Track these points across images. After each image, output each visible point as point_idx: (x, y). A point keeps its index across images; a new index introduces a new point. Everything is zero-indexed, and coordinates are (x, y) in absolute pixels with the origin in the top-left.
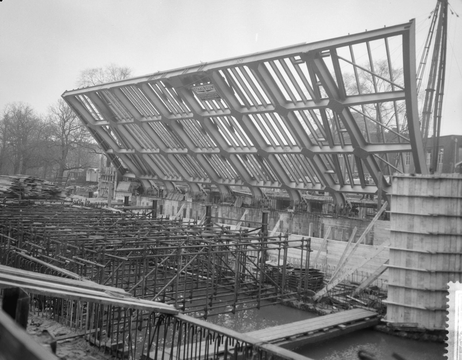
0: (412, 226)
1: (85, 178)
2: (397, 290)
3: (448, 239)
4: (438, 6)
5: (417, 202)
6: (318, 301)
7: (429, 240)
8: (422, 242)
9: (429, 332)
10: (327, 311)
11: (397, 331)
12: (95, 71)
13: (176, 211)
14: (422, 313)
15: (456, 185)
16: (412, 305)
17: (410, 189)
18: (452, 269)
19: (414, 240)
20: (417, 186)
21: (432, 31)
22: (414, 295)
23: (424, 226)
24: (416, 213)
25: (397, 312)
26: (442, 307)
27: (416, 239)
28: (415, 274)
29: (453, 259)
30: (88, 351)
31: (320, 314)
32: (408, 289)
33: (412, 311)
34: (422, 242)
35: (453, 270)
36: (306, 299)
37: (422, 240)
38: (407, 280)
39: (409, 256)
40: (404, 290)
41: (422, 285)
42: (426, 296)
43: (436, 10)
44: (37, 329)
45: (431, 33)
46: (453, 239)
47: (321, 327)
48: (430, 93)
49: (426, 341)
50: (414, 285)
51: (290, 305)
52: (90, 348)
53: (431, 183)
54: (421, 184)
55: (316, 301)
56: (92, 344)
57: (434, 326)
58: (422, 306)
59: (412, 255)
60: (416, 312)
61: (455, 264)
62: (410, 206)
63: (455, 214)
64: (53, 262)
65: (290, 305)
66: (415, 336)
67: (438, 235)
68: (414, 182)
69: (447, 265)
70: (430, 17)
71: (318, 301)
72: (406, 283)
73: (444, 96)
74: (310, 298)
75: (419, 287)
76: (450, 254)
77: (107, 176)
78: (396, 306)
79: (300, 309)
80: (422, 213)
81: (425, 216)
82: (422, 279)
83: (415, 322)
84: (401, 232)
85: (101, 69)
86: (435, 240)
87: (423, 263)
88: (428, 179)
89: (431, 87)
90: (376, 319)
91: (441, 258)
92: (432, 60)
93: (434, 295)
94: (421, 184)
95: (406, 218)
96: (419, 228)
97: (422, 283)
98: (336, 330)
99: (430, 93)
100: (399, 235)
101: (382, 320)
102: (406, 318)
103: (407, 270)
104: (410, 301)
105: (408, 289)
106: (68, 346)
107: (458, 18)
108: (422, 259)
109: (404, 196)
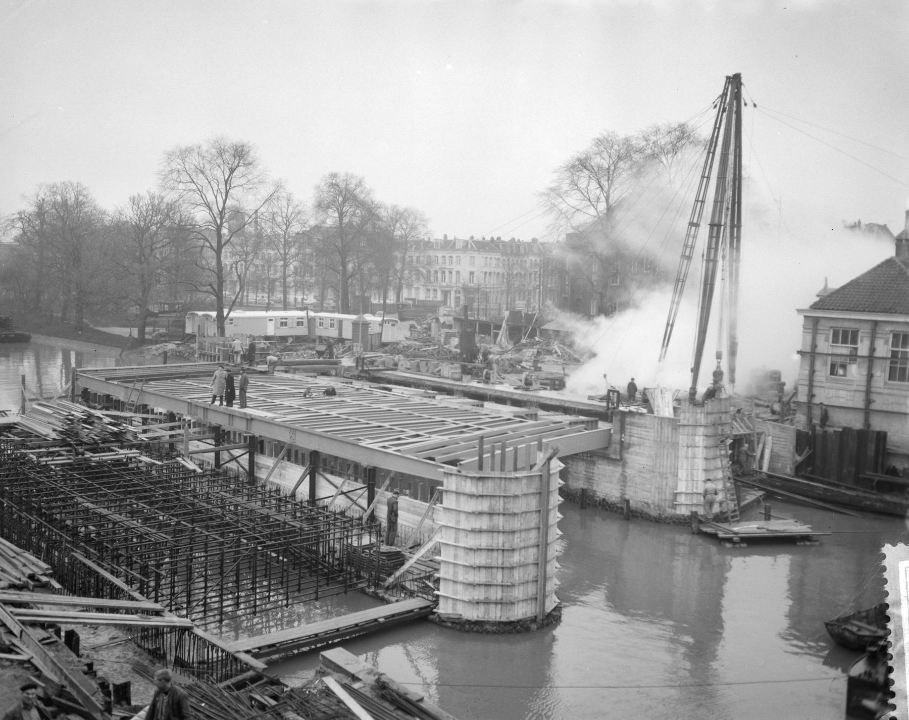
0: (458, 522)
3: (490, 534)
4: (726, 89)
5: (463, 499)
6: (391, 587)
7: (471, 536)
8: (467, 537)
9: (469, 622)
10: (394, 599)
11: (443, 621)
16: (458, 597)
17: (457, 485)
19: (461, 535)
20: (463, 483)
21: (718, 126)
22: (460, 588)
24: (461, 509)
25: (447, 602)
27: (462, 534)
28: (461, 568)
29: (495, 554)
30: (136, 652)
31: (388, 602)
32: (455, 582)
33: (458, 603)
36: (377, 586)
38: (455, 573)
40: (452, 583)
41: (467, 579)
42: (471, 589)
43: (724, 95)
44: (95, 633)
46: (495, 535)
47: (357, 622)
48: (715, 228)
49: (468, 631)
50: (460, 578)
52: (138, 650)
53: (474, 481)
54: (465, 481)
55: (388, 587)
56: (139, 646)
57: (478, 617)
58: (466, 598)
61: (497, 559)
63: (498, 511)
66: (458, 627)
67: (481, 531)
68: (460, 478)
71: (391, 587)
72: (454, 576)
73: (743, 229)
74: (382, 583)
75: (465, 581)
78: (447, 598)
79: (371, 596)
80: (467, 510)
81: (469, 513)
82: (467, 573)
83: (460, 613)
86: (478, 536)
87: (468, 558)
90: (429, 609)
91: (484, 553)
92: (718, 178)
93: (477, 588)
94: (465, 481)
95: (454, 513)
96: (465, 524)
98: (376, 623)
99: (715, 228)
101: (435, 610)
102: (454, 609)
103: (454, 564)
105: (455, 582)
106: (120, 648)
109: (452, 492)
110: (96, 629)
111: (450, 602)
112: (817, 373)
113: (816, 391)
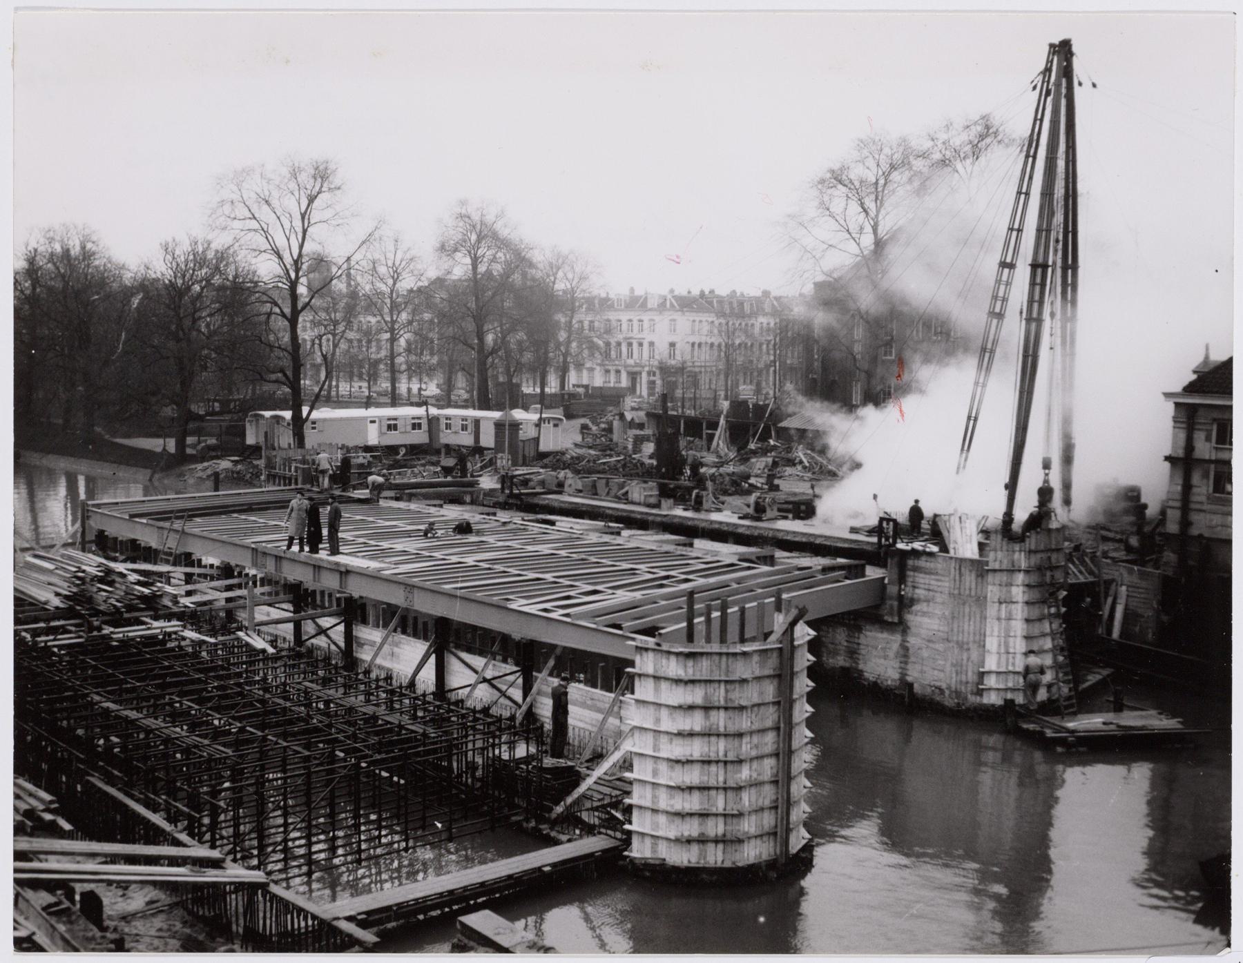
0: (658, 721)
1: (243, 435)
2: (643, 811)
3: (706, 739)
5: (664, 685)
7: (678, 741)
8: (671, 743)
10: (564, 838)
12: (247, 172)
13: (181, 849)
14: (672, 844)
15: (717, 661)
18: (712, 783)
22: (662, 819)
23: (674, 720)
24: (663, 702)
26: (699, 836)
27: (664, 739)
28: (664, 790)
29: (713, 768)
31: (556, 842)
32: (655, 811)
33: (660, 842)
34: (671, 743)
35: (715, 784)
37: (671, 741)
39: (655, 763)
41: (672, 806)
42: (678, 820)
43: (1048, 70)
45: (1038, 122)
46: (713, 739)
48: (1039, 271)
51: (519, 829)
57: (689, 862)
58: (672, 835)
59: (659, 762)
60: (665, 843)
61: (717, 775)
62: (657, 690)
63: (716, 704)
64: (138, 801)
65: (519, 829)
69: (706, 778)
70: (1034, 88)
72: (653, 802)
73: (1081, 272)
75: (669, 809)
76: (709, 762)
77: (280, 477)
78: (643, 835)
81: (674, 707)
82: (672, 797)
84: (646, 729)
85: (263, 166)
86: (688, 741)
87: (674, 775)
88: (678, 654)
89: (1041, 260)
94: (668, 659)
95: (652, 708)
97: (672, 802)
99: (1039, 271)
100: (643, 731)
102: (654, 851)
104: (658, 826)
105: (655, 811)
107: (1094, 89)
108: (672, 767)
110: (126, 888)
111: (648, 841)
112: (1195, 490)
113: (1194, 517)
